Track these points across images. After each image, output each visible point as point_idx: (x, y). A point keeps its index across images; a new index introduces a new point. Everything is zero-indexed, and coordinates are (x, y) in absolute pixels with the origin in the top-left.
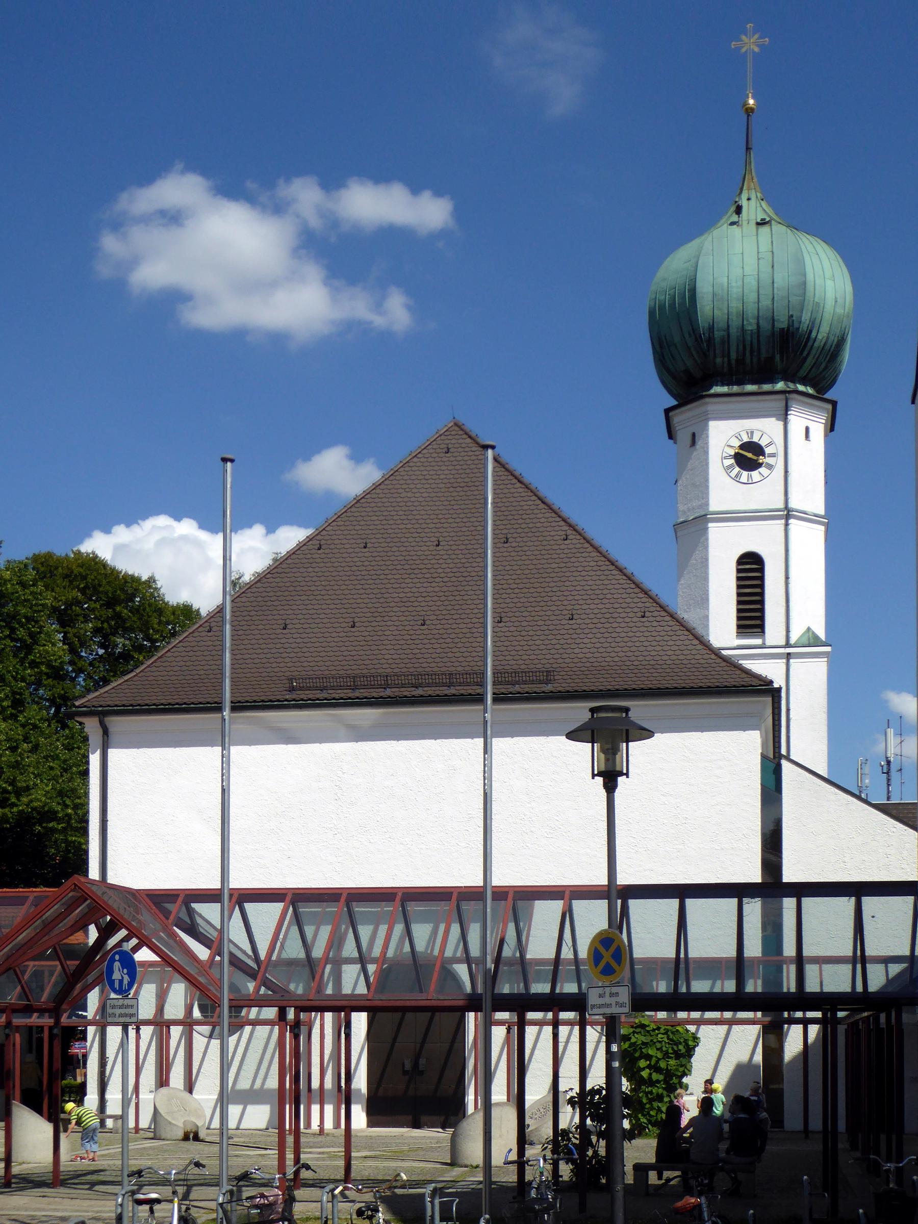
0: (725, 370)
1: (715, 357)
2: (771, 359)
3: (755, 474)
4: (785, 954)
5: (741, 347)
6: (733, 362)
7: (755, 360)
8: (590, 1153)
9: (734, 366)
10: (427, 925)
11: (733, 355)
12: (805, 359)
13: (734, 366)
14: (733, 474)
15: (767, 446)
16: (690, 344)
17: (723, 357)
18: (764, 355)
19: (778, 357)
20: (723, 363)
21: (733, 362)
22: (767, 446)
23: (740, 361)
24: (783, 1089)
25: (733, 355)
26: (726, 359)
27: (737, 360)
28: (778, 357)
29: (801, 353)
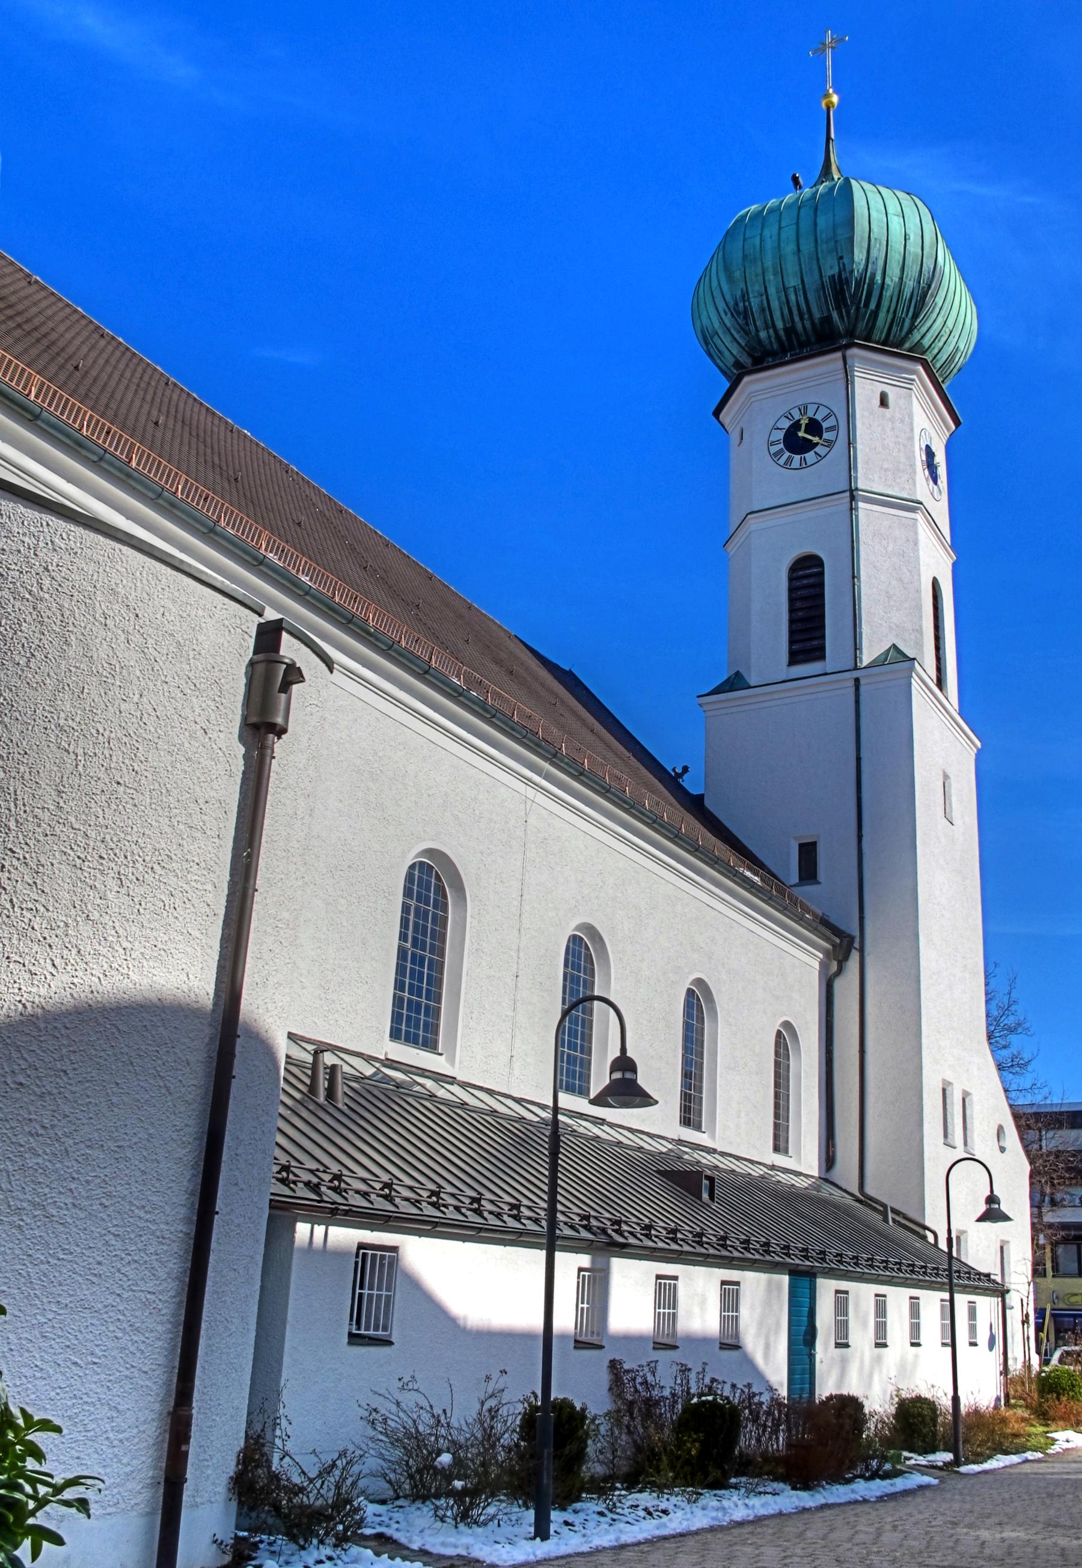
0: (775, 346)
1: (757, 331)
2: (827, 320)
3: (810, 456)
4: (282, 653)
5: (786, 311)
6: (782, 333)
7: (808, 324)
8: (618, 1485)
9: (784, 338)
10: (211, 989)
11: (780, 325)
12: (875, 314)
13: (784, 338)
14: (782, 461)
15: (825, 419)
16: (728, 324)
17: (767, 328)
18: (817, 315)
19: (835, 315)
20: (769, 337)
21: (782, 333)
22: (825, 419)
23: (790, 331)
24: (395, 989)
25: (780, 325)
26: (771, 331)
27: (786, 329)
28: (835, 315)
29: (867, 304)
